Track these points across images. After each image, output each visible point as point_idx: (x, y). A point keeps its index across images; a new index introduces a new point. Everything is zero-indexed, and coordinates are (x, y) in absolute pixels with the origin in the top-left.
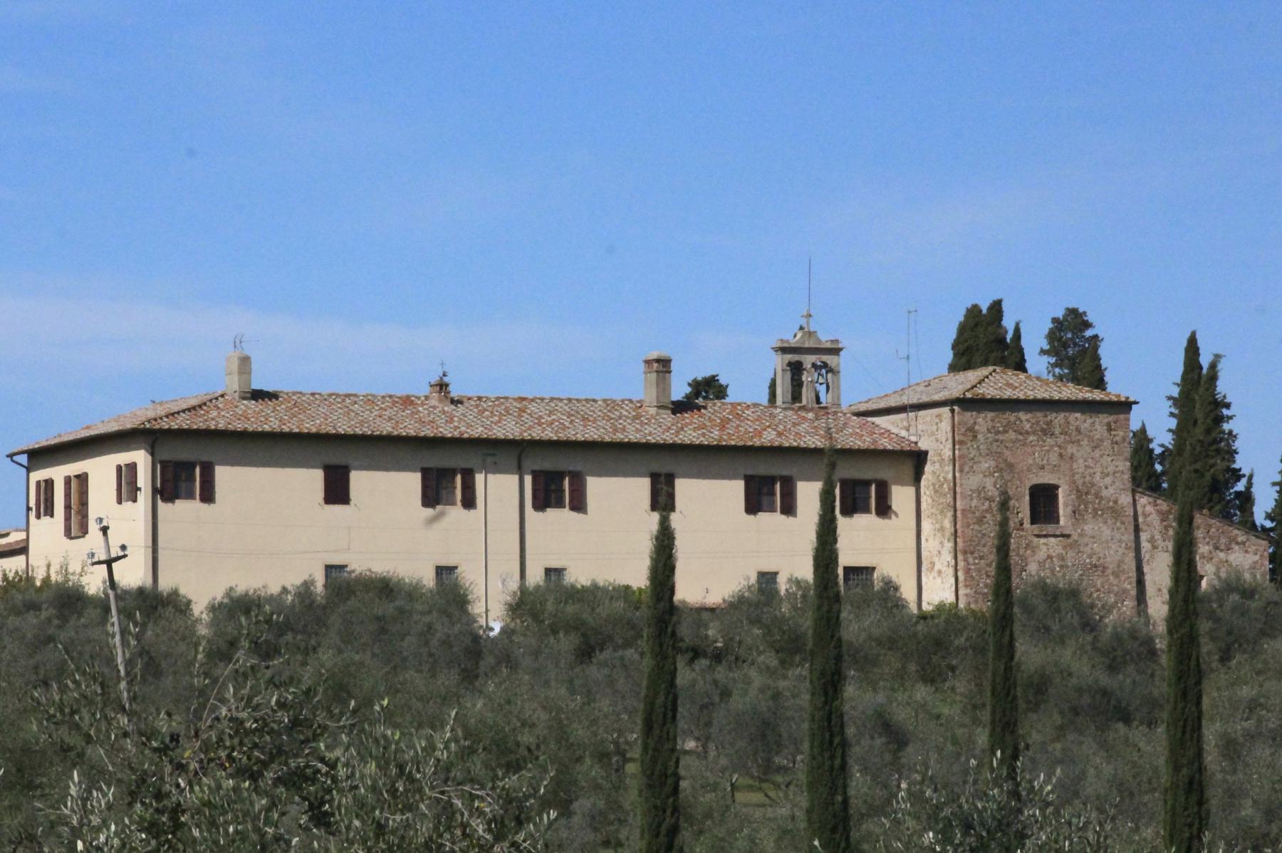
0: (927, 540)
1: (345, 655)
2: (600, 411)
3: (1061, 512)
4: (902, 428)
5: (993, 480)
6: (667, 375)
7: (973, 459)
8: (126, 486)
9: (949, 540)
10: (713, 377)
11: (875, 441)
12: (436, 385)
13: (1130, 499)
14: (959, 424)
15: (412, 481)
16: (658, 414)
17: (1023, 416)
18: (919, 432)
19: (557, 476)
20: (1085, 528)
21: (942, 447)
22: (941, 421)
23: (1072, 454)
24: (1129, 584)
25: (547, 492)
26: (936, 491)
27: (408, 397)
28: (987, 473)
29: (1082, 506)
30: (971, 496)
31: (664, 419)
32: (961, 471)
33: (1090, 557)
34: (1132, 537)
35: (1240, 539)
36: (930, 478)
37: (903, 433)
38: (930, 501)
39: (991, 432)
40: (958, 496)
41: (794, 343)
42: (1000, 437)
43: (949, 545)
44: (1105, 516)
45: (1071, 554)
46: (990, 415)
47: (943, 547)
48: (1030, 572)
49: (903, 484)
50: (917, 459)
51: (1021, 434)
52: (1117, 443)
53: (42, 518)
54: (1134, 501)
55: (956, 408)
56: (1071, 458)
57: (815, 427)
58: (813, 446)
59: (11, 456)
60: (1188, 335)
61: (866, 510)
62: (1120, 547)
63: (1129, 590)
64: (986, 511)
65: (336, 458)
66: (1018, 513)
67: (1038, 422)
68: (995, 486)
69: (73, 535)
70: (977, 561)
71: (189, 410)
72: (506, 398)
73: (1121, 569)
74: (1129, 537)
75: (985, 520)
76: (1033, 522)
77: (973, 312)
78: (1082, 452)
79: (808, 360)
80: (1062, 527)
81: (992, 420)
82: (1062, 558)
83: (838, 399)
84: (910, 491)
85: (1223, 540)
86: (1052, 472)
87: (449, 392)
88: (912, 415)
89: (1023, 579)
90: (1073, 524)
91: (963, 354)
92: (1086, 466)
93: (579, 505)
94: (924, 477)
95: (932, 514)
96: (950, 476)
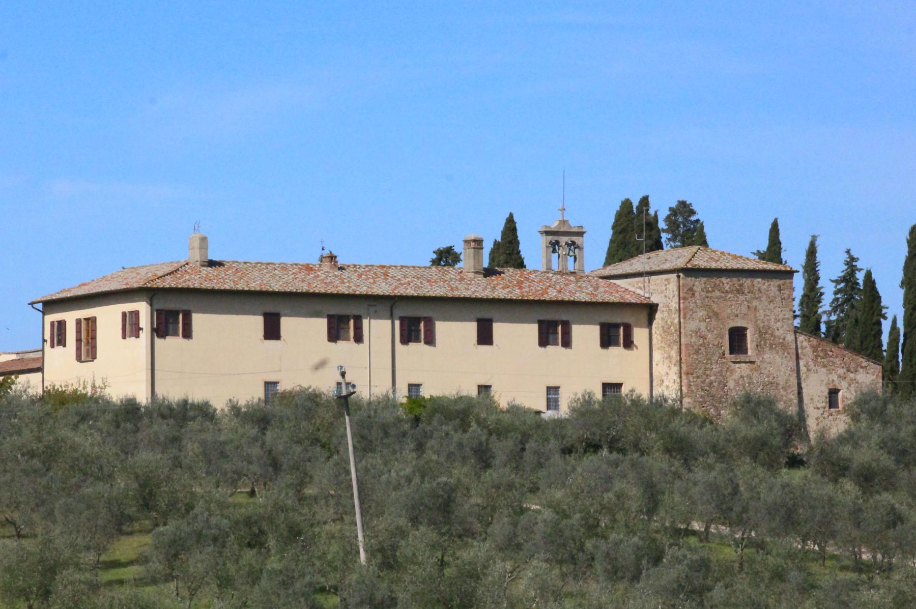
0: (657, 365)
1: (5, 445)
2: (436, 275)
3: (749, 346)
4: (637, 288)
5: (705, 324)
6: (481, 251)
7: (692, 310)
8: (130, 326)
9: (675, 365)
10: (451, 247)
11: (622, 298)
12: (328, 257)
13: (793, 337)
14: (683, 286)
15: (321, 324)
16: (475, 278)
17: (724, 280)
18: (651, 291)
19: (416, 321)
20: (765, 357)
21: (669, 301)
22: (669, 284)
23: (756, 307)
24: (793, 395)
25: (410, 331)
26: (664, 331)
27: (308, 265)
28: (701, 319)
29: (763, 342)
30: (691, 335)
31: (480, 281)
32: (685, 318)
33: (768, 377)
34: (795, 364)
35: (864, 365)
36: (660, 322)
37: (641, 292)
38: (659, 338)
39: (703, 292)
40: (682, 335)
41: (555, 228)
42: (710, 295)
43: (676, 369)
44: (777, 348)
45: (756, 374)
46: (704, 280)
47: (670, 369)
48: (729, 387)
49: (641, 327)
50: (651, 310)
51: (723, 292)
52: (784, 299)
53: (56, 347)
54: (796, 338)
55: (681, 275)
56: (755, 309)
57: (579, 287)
58: (584, 300)
59: (32, 304)
60: (772, 220)
61: (617, 344)
62: (787, 370)
63: (792, 400)
64: (701, 345)
65: (271, 307)
66: (721, 346)
67: (734, 285)
68: (707, 328)
69: (83, 359)
70: (695, 380)
71: (170, 274)
72: (372, 266)
73: (788, 385)
74: (793, 364)
75: (700, 351)
76: (731, 353)
77: (627, 204)
78: (761, 305)
79: (564, 240)
80: (749, 356)
81: (705, 283)
82: (750, 377)
83: (583, 266)
84: (645, 331)
85: (853, 365)
86: (743, 318)
87: (337, 262)
88: (647, 279)
89: (725, 392)
90: (757, 355)
91: (620, 233)
92: (765, 315)
93: (430, 340)
94: (655, 322)
95: (662, 347)
96: (676, 321)
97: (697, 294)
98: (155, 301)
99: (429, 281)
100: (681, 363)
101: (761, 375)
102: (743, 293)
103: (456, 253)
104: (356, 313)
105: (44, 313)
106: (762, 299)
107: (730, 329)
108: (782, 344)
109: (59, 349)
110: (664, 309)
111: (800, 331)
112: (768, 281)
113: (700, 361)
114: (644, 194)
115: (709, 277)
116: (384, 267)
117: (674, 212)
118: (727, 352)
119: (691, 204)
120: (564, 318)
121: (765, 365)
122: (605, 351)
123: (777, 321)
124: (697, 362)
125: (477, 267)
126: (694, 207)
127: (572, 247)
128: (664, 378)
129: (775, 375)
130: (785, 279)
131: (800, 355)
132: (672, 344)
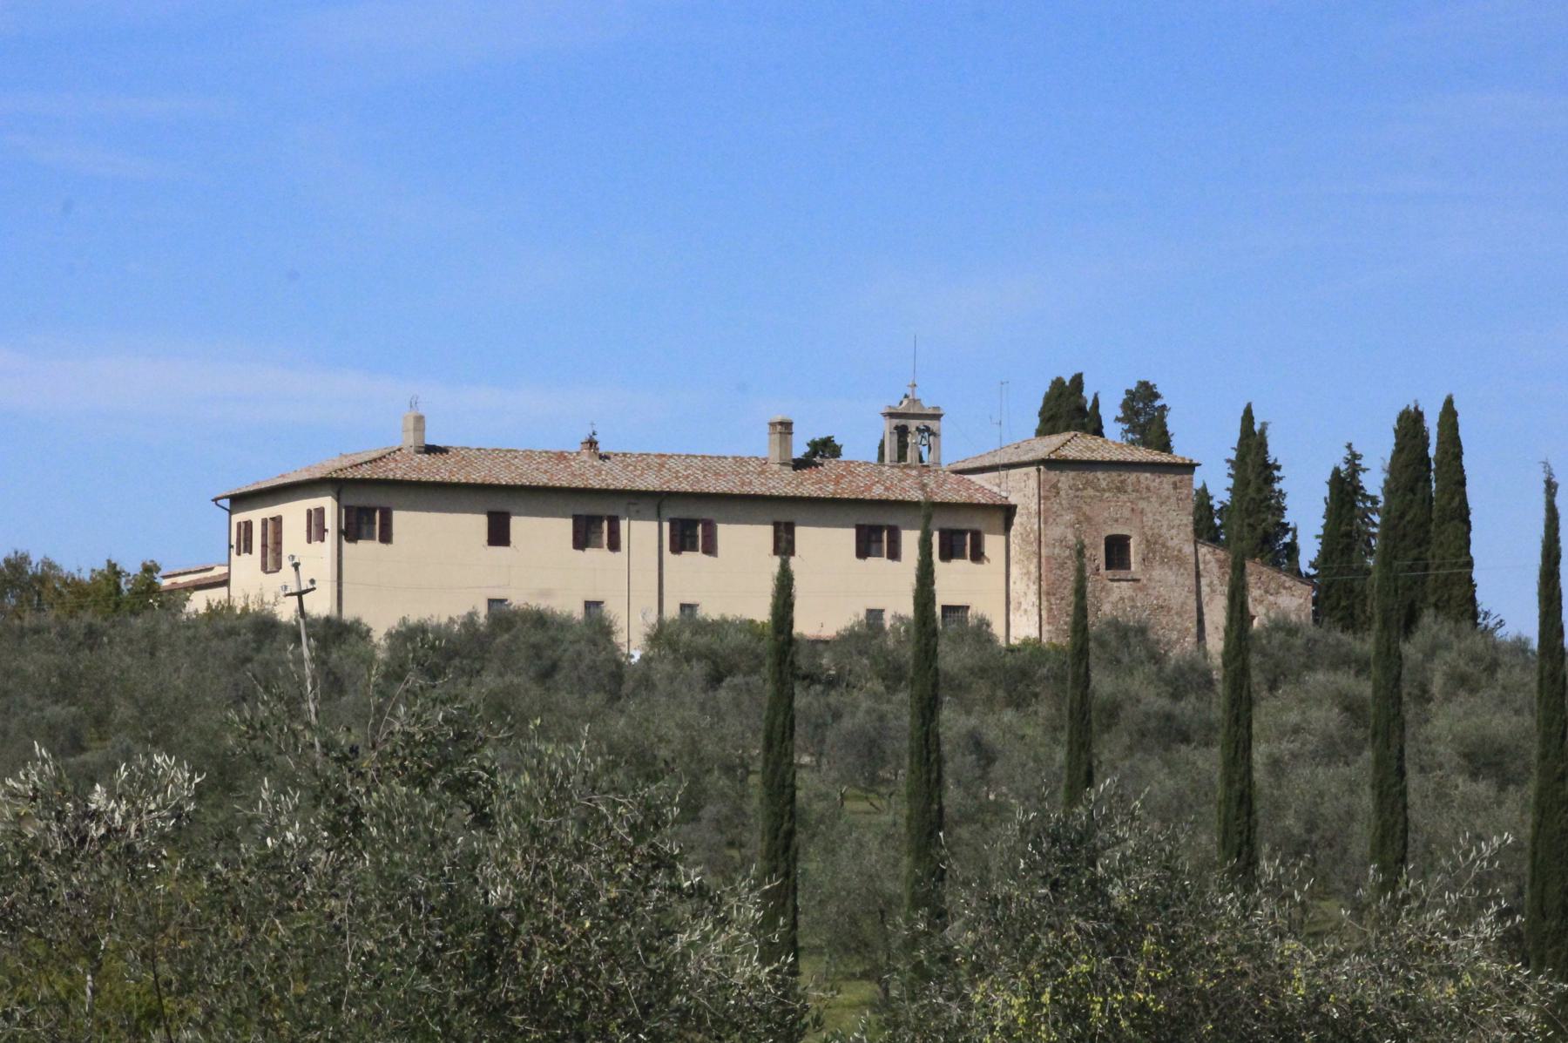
3: (1132, 559)
13: (1192, 549)
17: (1100, 475)
25: (683, 537)
26: (1023, 540)
27: (562, 453)
32: (1046, 523)
35: (1287, 585)
42: (1079, 493)
43: (1034, 588)
45: (1140, 595)
46: (1072, 474)
56: (1142, 512)
59: (215, 500)
71: (370, 462)
72: (648, 455)
74: (1191, 581)
76: (1109, 566)
78: (1150, 507)
79: (913, 424)
82: (1132, 599)
85: (1273, 585)
86: (1125, 524)
93: (710, 549)
96: (1036, 527)
97: (1062, 493)
98: (343, 496)
99: (716, 474)
100: (1040, 580)
104: (611, 513)
105: (231, 513)
108: (1178, 558)
109: (245, 556)
116: (664, 456)
117: (1132, 396)
120: (892, 522)
122: (861, 562)
123: (1171, 527)
131: (1202, 572)
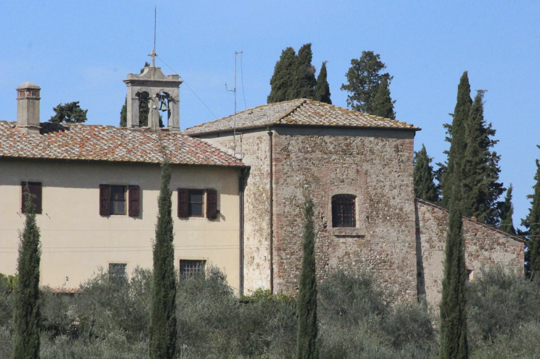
0: (248, 239)
3: (357, 217)
4: (229, 148)
6: (36, 101)
7: (286, 173)
9: (266, 239)
10: (75, 103)
13: (412, 207)
16: (28, 133)
17: (327, 138)
18: (243, 151)
21: (261, 163)
22: (261, 142)
23: (367, 171)
31: (33, 137)
32: (277, 183)
34: (414, 238)
35: (501, 241)
36: (252, 188)
38: (251, 207)
39: (301, 152)
40: (274, 203)
42: (308, 156)
43: (266, 243)
45: (365, 251)
46: (301, 138)
48: (331, 266)
49: (229, 193)
52: (403, 162)
54: (416, 209)
55: (273, 131)
60: (461, 75)
61: (199, 214)
66: (322, 218)
70: (288, 256)
76: (334, 225)
79: (153, 91)
82: (357, 254)
83: (178, 123)
85: (487, 242)
86: (350, 184)
88: (237, 137)
92: (377, 180)
94: (247, 188)
96: (268, 187)
101: (372, 252)
102: (351, 154)
103: (81, 111)
106: (374, 162)
107: (333, 197)
108: (399, 216)
110: (256, 173)
111: (421, 200)
112: (382, 141)
113: (294, 235)
114: (306, 43)
115: (308, 135)
117: (357, 65)
118: (330, 224)
119: (378, 55)
120: (133, 182)
121: (377, 240)
124: (291, 235)
125: (31, 122)
126: (382, 60)
127: (166, 100)
128: (255, 254)
129: (389, 253)
130: (403, 138)
131: (421, 229)
132: (264, 214)
